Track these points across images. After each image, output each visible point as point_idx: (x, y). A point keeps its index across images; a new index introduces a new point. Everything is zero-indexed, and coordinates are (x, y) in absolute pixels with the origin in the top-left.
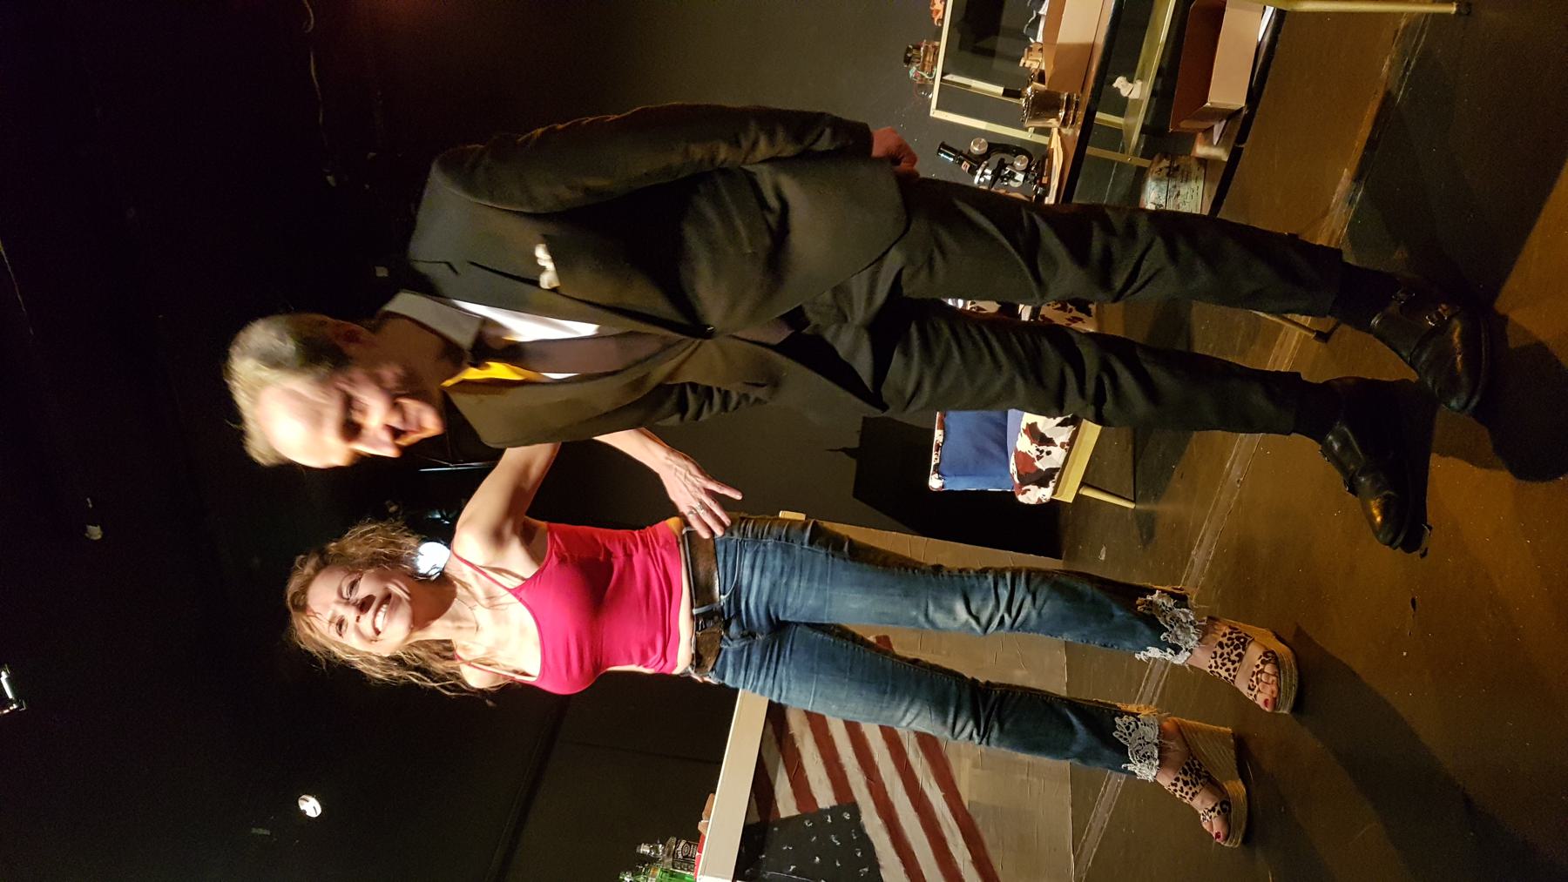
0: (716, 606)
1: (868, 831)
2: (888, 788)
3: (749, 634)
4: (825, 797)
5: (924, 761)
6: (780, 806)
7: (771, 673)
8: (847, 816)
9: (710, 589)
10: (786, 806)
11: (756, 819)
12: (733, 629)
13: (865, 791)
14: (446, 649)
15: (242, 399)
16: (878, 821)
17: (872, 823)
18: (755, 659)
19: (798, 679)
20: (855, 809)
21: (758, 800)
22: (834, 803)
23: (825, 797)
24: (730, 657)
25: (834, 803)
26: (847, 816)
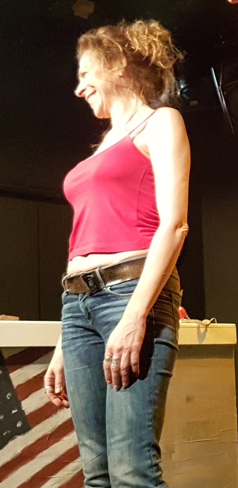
0: (102, 285)
1: (11, 443)
2: (45, 452)
3: (90, 315)
4: (30, 404)
5: (71, 476)
6: (18, 372)
7: (75, 336)
8: (19, 425)
9: (113, 278)
10: (19, 376)
11: (6, 355)
12: (90, 301)
13: (40, 435)
14: (98, 36)
15: (78, 51)
16: (19, 450)
17: (17, 445)
18: (79, 323)
19: (79, 356)
20: (25, 429)
21: (19, 353)
22: (27, 412)
23: (30, 404)
24: (75, 303)
25: (27, 412)
26: (19, 425)
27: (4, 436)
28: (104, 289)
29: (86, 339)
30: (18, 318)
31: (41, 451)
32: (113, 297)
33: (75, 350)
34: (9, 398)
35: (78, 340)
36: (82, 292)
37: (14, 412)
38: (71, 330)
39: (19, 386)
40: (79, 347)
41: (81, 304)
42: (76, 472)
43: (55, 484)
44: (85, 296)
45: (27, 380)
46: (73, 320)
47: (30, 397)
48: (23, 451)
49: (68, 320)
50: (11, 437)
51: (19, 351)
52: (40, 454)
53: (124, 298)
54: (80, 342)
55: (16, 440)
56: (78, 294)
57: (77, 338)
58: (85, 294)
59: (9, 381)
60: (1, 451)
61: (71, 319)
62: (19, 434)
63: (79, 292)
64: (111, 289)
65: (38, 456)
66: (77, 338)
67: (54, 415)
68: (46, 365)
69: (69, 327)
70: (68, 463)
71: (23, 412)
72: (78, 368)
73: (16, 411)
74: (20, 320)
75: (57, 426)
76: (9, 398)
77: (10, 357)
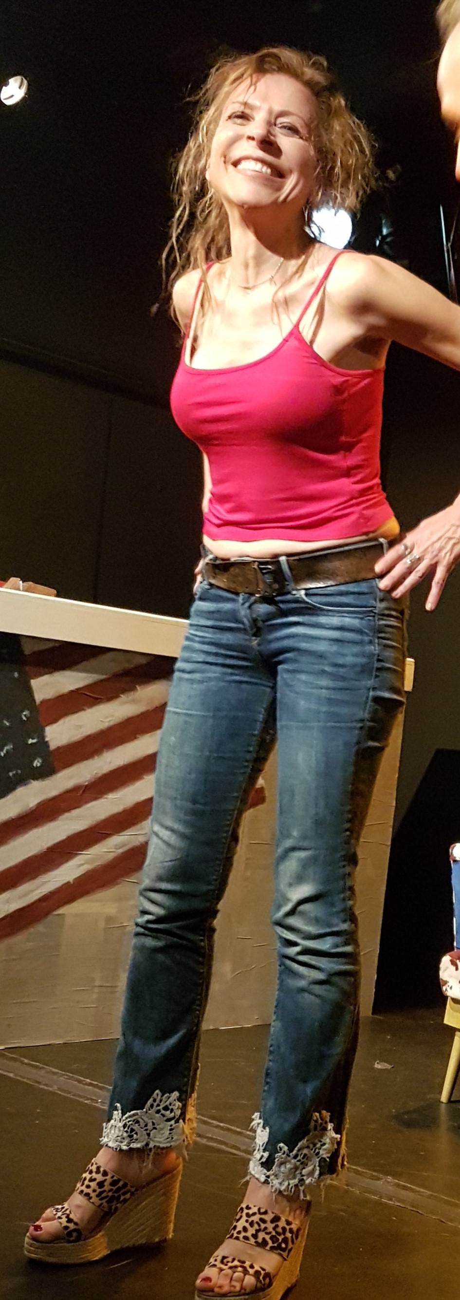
0: (291, 585)
1: (20, 791)
2: (75, 812)
4: (59, 734)
5: (111, 856)
6: (46, 678)
7: (210, 659)
8: (37, 763)
9: (313, 575)
10: (47, 686)
12: (263, 609)
13: (70, 784)
17: (30, 795)
21: (53, 649)
22: (53, 746)
23: (59, 734)
24: (228, 606)
25: (53, 746)
26: (37, 763)
27: (9, 777)
28: (294, 592)
29: (229, 671)
30: (55, 592)
31: (69, 810)
32: (310, 608)
33: (201, 682)
34: (24, 718)
35: (213, 668)
36: (247, 590)
37: (30, 741)
38: (206, 648)
39: (44, 702)
40: (210, 679)
41: (243, 612)
42: (120, 851)
43: (83, 865)
44: (253, 598)
45: (57, 694)
46: (214, 633)
47: (61, 722)
48: (39, 805)
49: (203, 629)
50: (21, 781)
51: (51, 645)
52: (67, 815)
53: (330, 613)
54: (214, 673)
55: (29, 786)
56: (237, 594)
57: (216, 664)
58: (252, 594)
59: (29, 691)
60: (4, 800)
61: (211, 630)
62: (36, 778)
63: (239, 589)
64: (306, 595)
65: (62, 817)
66: (216, 664)
67: (96, 757)
68: (23, 641)
69: (203, 643)
70: (109, 835)
71: (46, 744)
72: (195, 713)
73: (35, 741)
74: (58, 596)
75: (99, 775)
76: (24, 718)
77: (34, 653)
